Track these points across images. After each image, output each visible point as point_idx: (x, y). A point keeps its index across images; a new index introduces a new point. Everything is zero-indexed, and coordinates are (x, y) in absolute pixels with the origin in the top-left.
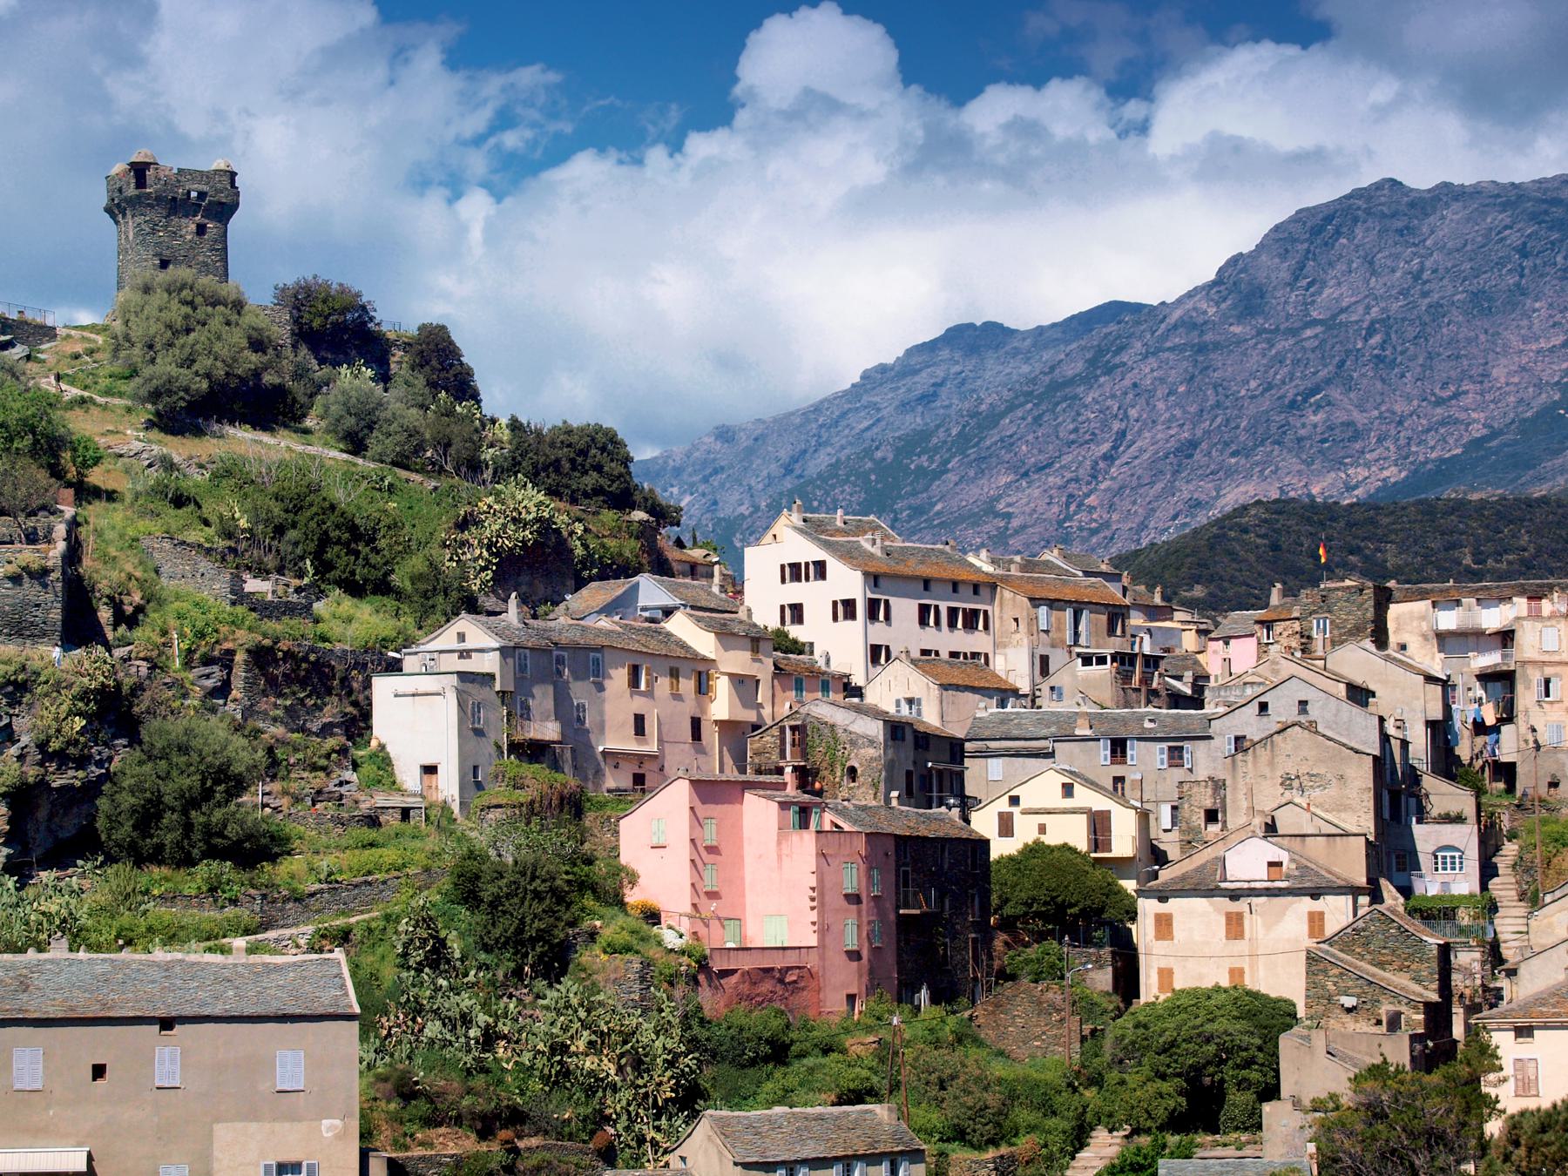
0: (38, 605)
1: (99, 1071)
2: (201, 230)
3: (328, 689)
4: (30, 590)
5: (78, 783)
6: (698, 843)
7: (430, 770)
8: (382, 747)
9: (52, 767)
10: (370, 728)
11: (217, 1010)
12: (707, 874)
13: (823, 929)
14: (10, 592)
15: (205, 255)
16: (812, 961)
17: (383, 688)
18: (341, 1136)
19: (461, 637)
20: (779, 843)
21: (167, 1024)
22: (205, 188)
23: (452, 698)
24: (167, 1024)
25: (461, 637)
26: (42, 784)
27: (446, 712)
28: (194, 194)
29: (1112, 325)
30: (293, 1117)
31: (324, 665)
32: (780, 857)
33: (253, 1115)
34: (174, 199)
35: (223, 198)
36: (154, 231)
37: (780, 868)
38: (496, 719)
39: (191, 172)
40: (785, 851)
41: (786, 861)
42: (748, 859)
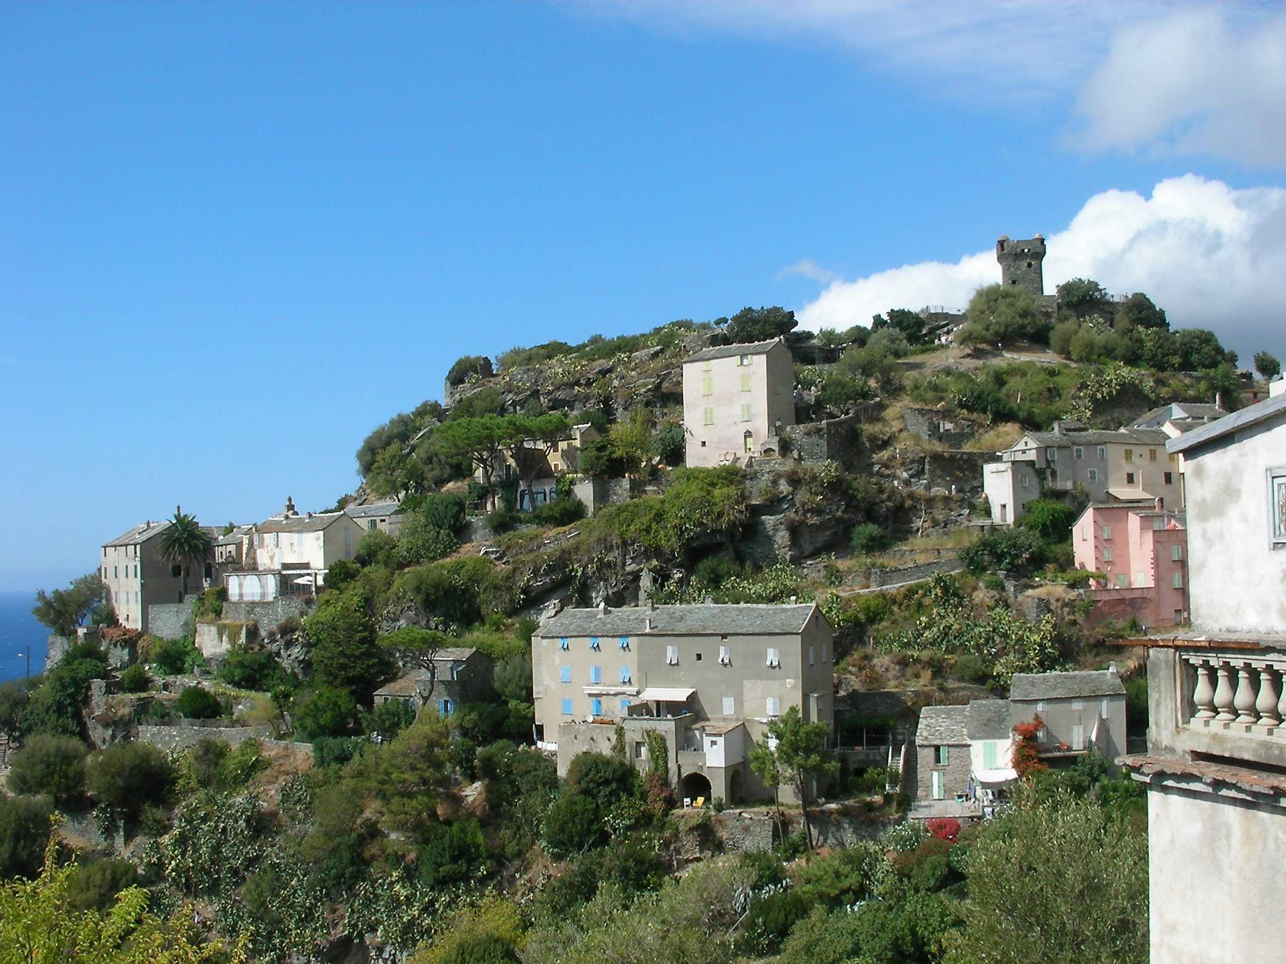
1: (699, 657)
2: (1030, 265)
3: (966, 471)
4: (815, 439)
7: (1004, 506)
10: (982, 486)
11: (744, 631)
12: (1106, 553)
13: (1158, 578)
16: (1151, 595)
17: (988, 468)
18: (794, 687)
21: (724, 636)
23: (1009, 475)
24: (724, 636)
26: (803, 523)
27: (1008, 478)
29: (913, 329)
30: (775, 678)
33: (759, 677)
38: (1031, 480)
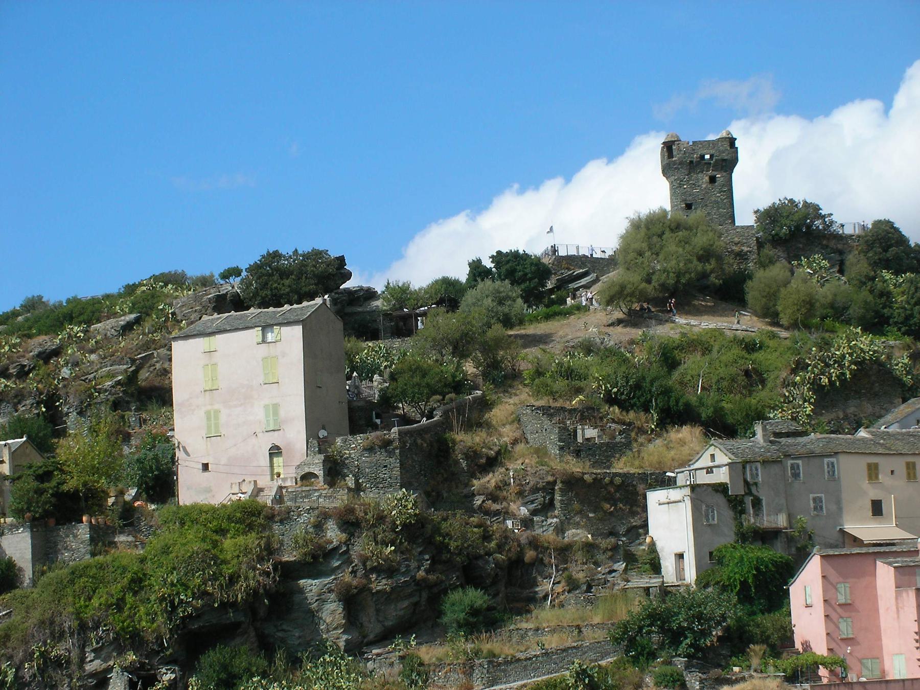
0: (386, 466)
2: (713, 180)
5: (388, 588)
6: (833, 602)
7: (680, 556)
8: (653, 544)
9: (373, 577)
14: (368, 459)
15: (716, 195)
17: (654, 498)
19: (713, 456)
20: (897, 598)
22: (712, 152)
25: (713, 456)
27: (685, 512)
28: (707, 157)
31: (628, 485)
32: (897, 609)
34: (691, 162)
35: (725, 156)
36: (680, 186)
37: (898, 617)
38: (723, 514)
39: (701, 142)
40: (900, 605)
41: (901, 611)
42: (882, 611)
